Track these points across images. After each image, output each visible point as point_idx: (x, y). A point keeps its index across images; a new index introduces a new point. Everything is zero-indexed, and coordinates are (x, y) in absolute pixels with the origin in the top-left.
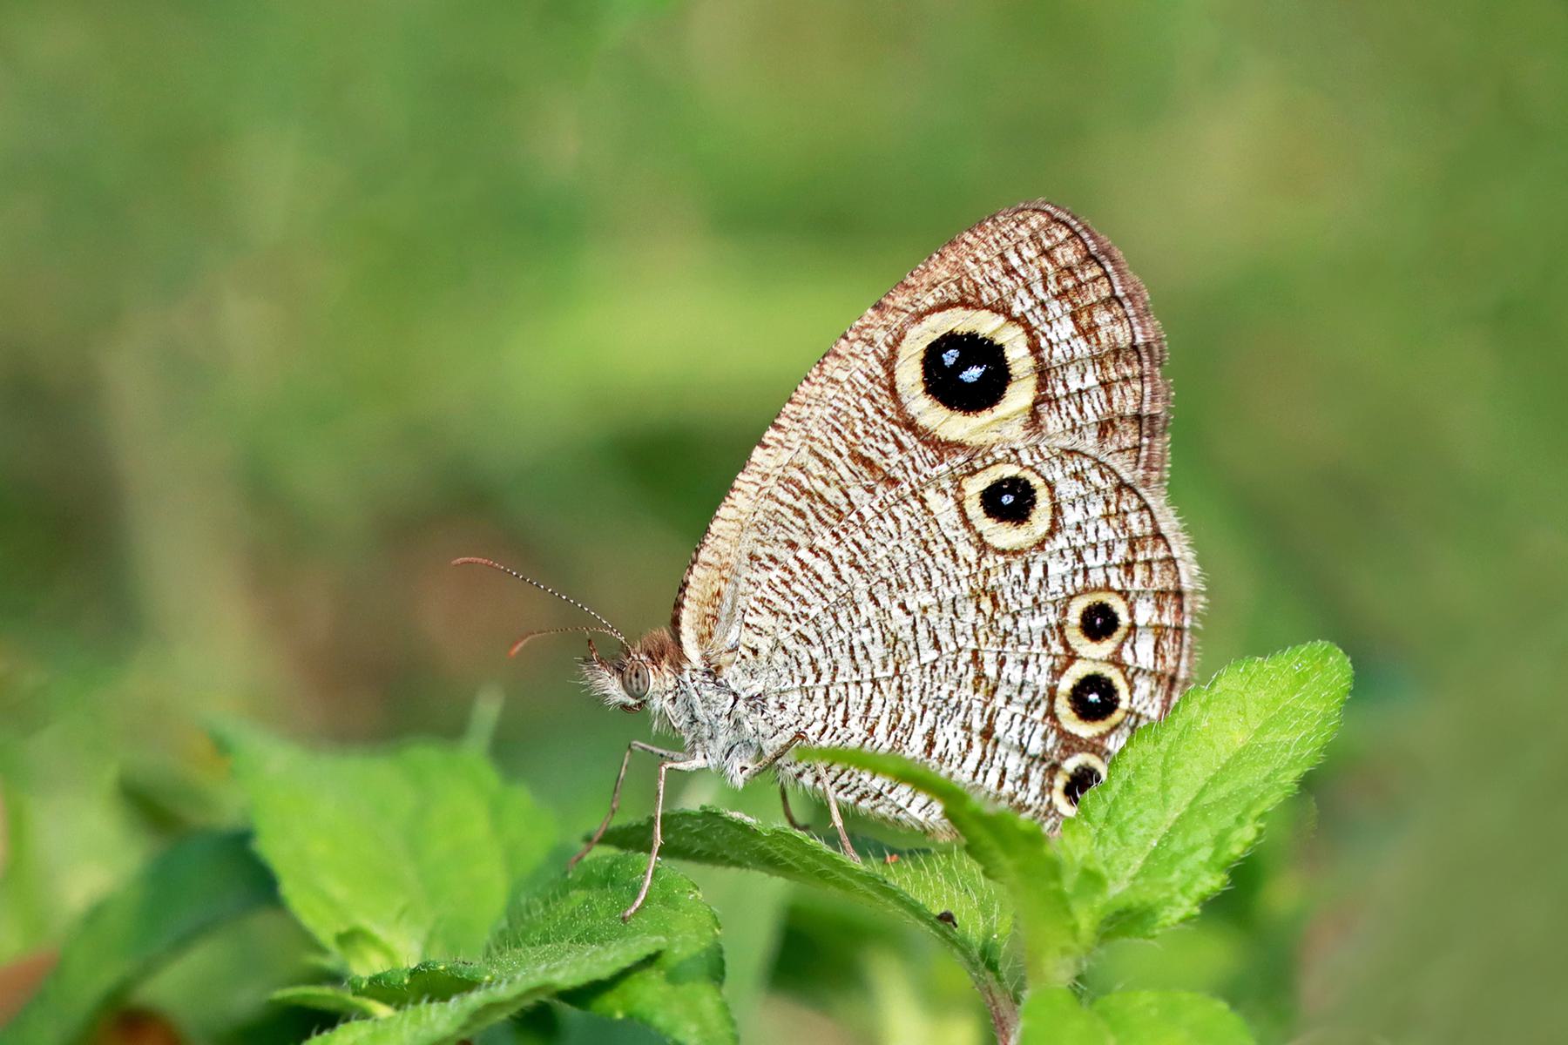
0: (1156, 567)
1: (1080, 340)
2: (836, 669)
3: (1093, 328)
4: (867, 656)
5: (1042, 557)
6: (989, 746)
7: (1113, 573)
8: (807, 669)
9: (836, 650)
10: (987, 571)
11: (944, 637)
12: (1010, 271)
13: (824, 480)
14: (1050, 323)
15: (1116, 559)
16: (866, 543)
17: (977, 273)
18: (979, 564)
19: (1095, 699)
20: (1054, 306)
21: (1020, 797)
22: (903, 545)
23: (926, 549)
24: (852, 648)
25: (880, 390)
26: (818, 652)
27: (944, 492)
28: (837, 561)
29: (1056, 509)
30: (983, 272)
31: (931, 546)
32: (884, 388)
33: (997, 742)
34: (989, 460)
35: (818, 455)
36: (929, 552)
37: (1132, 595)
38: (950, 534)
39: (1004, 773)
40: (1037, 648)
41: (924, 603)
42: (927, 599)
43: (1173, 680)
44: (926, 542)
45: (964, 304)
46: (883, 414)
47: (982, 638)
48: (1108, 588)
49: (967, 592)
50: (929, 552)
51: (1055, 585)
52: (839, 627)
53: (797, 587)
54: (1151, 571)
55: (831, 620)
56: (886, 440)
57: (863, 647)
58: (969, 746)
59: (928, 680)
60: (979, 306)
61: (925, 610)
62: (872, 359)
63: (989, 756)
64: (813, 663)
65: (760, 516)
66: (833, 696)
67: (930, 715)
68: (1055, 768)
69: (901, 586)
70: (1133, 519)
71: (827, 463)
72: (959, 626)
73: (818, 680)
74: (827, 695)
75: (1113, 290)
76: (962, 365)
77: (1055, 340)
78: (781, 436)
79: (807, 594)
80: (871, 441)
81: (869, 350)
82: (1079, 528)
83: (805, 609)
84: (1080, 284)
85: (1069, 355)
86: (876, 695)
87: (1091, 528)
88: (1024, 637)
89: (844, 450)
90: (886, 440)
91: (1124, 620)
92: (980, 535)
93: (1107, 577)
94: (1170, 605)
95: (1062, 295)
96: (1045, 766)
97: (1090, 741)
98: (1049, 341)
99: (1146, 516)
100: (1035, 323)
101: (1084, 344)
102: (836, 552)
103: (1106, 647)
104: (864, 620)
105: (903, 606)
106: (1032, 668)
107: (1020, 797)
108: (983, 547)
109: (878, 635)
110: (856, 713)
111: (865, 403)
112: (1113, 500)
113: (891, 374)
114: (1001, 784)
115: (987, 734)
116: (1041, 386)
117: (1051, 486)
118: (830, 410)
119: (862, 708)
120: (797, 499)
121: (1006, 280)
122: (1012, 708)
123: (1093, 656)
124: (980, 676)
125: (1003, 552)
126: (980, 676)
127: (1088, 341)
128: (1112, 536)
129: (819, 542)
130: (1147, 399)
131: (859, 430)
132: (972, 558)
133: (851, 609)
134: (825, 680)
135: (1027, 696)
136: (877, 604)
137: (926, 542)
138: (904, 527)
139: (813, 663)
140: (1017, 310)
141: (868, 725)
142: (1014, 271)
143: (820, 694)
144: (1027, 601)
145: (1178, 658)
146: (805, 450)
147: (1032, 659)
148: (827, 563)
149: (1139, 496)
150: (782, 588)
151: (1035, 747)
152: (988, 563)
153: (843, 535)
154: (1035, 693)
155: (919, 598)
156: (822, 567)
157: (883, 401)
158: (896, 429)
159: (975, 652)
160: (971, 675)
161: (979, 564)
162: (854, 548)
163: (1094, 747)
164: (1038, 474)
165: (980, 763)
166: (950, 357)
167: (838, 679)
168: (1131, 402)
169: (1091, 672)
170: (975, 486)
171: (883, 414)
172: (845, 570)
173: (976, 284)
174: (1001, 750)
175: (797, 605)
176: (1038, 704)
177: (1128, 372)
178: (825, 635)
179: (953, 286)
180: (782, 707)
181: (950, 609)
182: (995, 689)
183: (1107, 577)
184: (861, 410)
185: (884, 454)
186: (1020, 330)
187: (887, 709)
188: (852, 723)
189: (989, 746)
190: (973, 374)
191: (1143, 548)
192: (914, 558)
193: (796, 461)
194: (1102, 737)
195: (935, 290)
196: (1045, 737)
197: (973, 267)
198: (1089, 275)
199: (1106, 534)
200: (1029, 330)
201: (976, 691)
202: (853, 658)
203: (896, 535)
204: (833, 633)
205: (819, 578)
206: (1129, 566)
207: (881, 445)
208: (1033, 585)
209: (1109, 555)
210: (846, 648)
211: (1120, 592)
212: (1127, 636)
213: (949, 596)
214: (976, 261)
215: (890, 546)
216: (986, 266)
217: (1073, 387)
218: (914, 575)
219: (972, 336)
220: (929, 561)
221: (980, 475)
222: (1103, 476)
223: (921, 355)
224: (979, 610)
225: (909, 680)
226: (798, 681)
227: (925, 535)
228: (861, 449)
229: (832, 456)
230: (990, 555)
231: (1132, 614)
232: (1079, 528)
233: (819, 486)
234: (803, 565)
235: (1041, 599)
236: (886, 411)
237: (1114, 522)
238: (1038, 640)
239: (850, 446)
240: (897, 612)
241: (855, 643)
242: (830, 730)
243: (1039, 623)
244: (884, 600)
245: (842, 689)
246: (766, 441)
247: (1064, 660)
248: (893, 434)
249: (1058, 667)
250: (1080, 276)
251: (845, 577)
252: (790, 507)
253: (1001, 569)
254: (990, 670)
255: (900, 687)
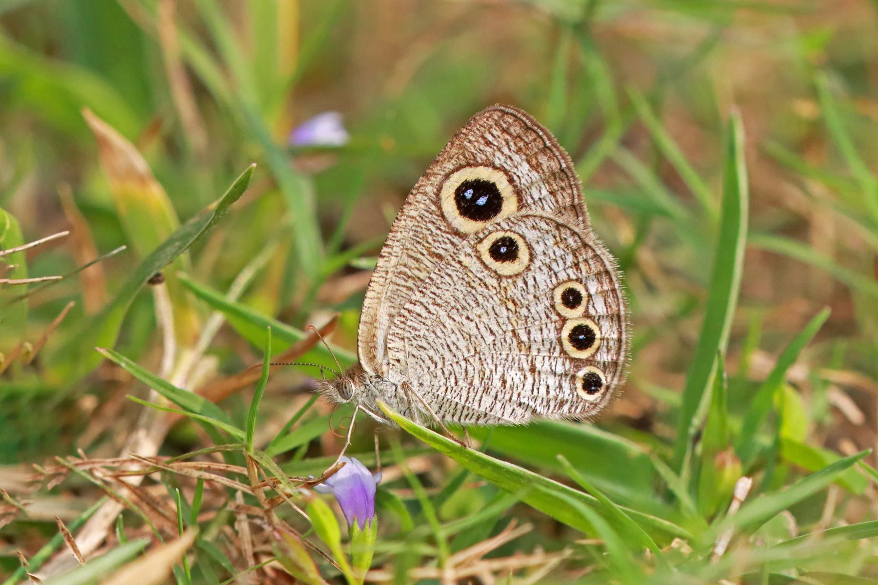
0: (591, 262)
1: (534, 173)
2: (444, 358)
3: (539, 165)
4: (457, 348)
5: (530, 274)
6: (536, 376)
7: (570, 271)
8: (429, 363)
9: (440, 349)
10: (505, 288)
11: (495, 328)
12: (488, 143)
13: (419, 269)
14: (516, 167)
15: (569, 264)
16: (438, 292)
17: (472, 147)
18: (500, 286)
19: (582, 338)
20: (516, 158)
21: (560, 397)
22: (457, 287)
23: (470, 286)
24: (448, 346)
25: (436, 217)
26: (431, 353)
27: (470, 255)
28: (426, 305)
29: (530, 247)
30: (475, 147)
31: (472, 284)
32: (438, 216)
33: (539, 373)
34: (486, 232)
35: (412, 257)
36: (473, 287)
37: (584, 280)
38: (480, 275)
39: (548, 387)
40: (544, 320)
41: (478, 313)
42: (479, 311)
43: (619, 316)
44: (469, 283)
45: (469, 165)
46: (440, 229)
47: (515, 324)
48: (570, 280)
49: (498, 302)
50: (473, 287)
51: (542, 286)
52: (438, 337)
53: (409, 323)
54: (589, 265)
55: (432, 335)
56: (445, 243)
57: (454, 344)
58: (525, 377)
59: (494, 352)
60: (477, 164)
61: (480, 317)
62: (428, 202)
63: (537, 380)
64: (431, 358)
65: (389, 294)
66: (447, 373)
67: (500, 369)
68: (574, 377)
69: (464, 308)
70: (571, 241)
71: (417, 260)
72: (501, 321)
73: (436, 367)
74: (443, 373)
75: (545, 144)
76: (475, 198)
77: (520, 175)
78: (390, 250)
79: (415, 325)
80: (437, 244)
81: (426, 198)
82: (545, 254)
83: (417, 333)
84: (527, 144)
85: (529, 181)
86: (469, 366)
87: (551, 252)
88: (536, 317)
89: (425, 252)
90: (445, 243)
91: (584, 293)
92: (496, 272)
93: (568, 275)
94: (605, 280)
95: (519, 151)
96: (568, 378)
97: (587, 360)
98: (518, 176)
99: (577, 238)
100: (508, 168)
101: (536, 174)
102: (424, 300)
103: (580, 310)
104: (450, 330)
105: (468, 318)
106: (545, 331)
107: (560, 397)
108: (499, 277)
109: (459, 336)
110: (461, 377)
111: (430, 226)
112: (557, 234)
113: (440, 208)
114: (548, 392)
115: (533, 370)
116: (520, 200)
117: (523, 237)
118: (412, 233)
119: (464, 374)
120: (406, 281)
121: (487, 149)
122: (542, 354)
123: (575, 317)
124: (520, 343)
125: (510, 277)
126: (520, 343)
127: (538, 172)
128: (563, 253)
129: (414, 298)
130: (576, 197)
131: (430, 239)
132: (496, 285)
133: (442, 327)
134: (440, 365)
135: (548, 346)
136: (454, 321)
137: (469, 283)
138: (455, 278)
139: (431, 358)
140: (497, 163)
141: (469, 381)
142: (491, 143)
143: (439, 373)
144: (531, 297)
145: (618, 305)
146: (404, 256)
147: (544, 326)
148: (421, 307)
149: (570, 229)
150: (402, 326)
151: (560, 369)
152: (504, 284)
153: (424, 290)
154: (551, 343)
155: (475, 312)
156: (418, 309)
157: (439, 223)
158: (449, 236)
159: (513, 331)
160: (515, 343)
161: (500, 286)
162: (433, 296)
163: (590, 362)
164: (514, 232)
165: (533, 385)
166: (469, 194)
167: (446, 363)
168: (568, 200)
169: (576, 325)
170: (484, 248)
171: (440, 229)
172: (432, 308)
173: (472, 153)
174: (543, 376)
175: (413, 332)
176: (554, 348)
177: (563, 184)
178: (432, 343)
179: (461, 157)
180: (421, 384)
181: (493, 313)
182: (530, 347)
183: (568, 275)
184: (429, 230)
185: (446, 250)
186: (502, 173)
187: (477, 371)
188: (460, 383)
189: (536, 376)
190: (482, 201)
191: (581, 254)
192: (465, 292)
193: (401, 262)
194: (593, 356)
195: (453, 161)
196: (564, 364)
197: (469, 144)
198: (531, 138)
199: (559, 252)
200: (506, 172)
201: (520, 351)
202: (451, 351)
203: (452, 284)
204: (436, 341)
205: (419, 315)
206: (576, 265)
207: (443, 246)
208: (531, 289)
209: (565, 263)
210: (445, 347)
211: (577, 280)
212: (588, 301)
213: (490, 306)
214: (470, 142)
215: (451, 289)
216: (476, 144)
217: (536, 197)
218: (468, 301)
219: (477, 182)
220: (473, 292)
221: (485, 241)
222: (547, 224)
223: (453, 196)
224: (508, 309)
225: (484, 354)
226: (426, 370)
227: (467, 279)
228: (433, 250)
229: (419, 256)
230: (504, 280)
231: (587, 290)
232: (545, 254)
233: (417, 272)
234: (409, 311)
235: (538, 295)
236: (442, 228)
237: (562, 246)
238: (544, 316)
239: (428, 249)
240: (465, 322)
241: (449, 343)
242: (449, 389)
243: (541, 308)
244: (457, 318)
245: (450, 368)
246: (383, 254)
247: (560, 323)
248: (448, 239)
249: (558, 327)
250: (526, 140)
251: (433, 311)
252: (404, 286)
253: (512, 286)
254: (524, 338)
255: (480, 359)
